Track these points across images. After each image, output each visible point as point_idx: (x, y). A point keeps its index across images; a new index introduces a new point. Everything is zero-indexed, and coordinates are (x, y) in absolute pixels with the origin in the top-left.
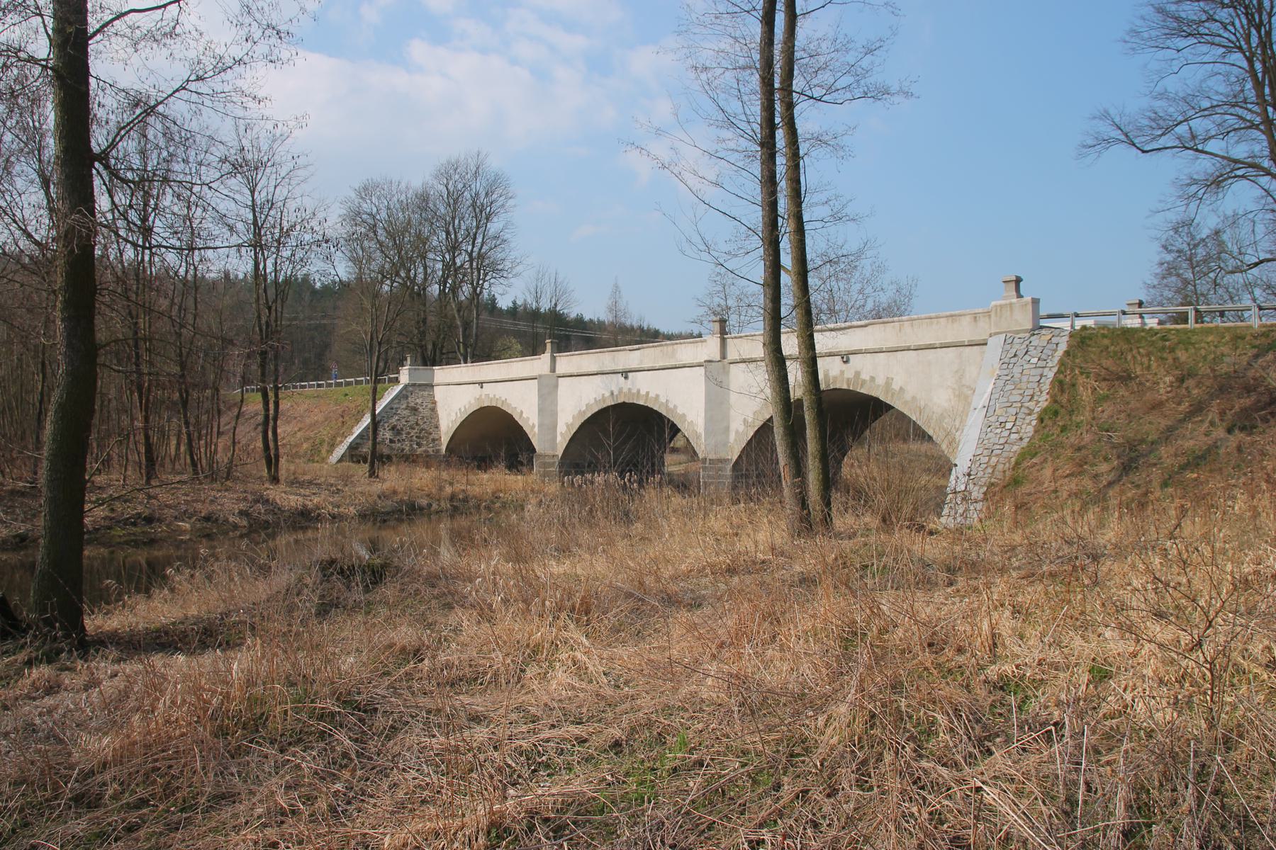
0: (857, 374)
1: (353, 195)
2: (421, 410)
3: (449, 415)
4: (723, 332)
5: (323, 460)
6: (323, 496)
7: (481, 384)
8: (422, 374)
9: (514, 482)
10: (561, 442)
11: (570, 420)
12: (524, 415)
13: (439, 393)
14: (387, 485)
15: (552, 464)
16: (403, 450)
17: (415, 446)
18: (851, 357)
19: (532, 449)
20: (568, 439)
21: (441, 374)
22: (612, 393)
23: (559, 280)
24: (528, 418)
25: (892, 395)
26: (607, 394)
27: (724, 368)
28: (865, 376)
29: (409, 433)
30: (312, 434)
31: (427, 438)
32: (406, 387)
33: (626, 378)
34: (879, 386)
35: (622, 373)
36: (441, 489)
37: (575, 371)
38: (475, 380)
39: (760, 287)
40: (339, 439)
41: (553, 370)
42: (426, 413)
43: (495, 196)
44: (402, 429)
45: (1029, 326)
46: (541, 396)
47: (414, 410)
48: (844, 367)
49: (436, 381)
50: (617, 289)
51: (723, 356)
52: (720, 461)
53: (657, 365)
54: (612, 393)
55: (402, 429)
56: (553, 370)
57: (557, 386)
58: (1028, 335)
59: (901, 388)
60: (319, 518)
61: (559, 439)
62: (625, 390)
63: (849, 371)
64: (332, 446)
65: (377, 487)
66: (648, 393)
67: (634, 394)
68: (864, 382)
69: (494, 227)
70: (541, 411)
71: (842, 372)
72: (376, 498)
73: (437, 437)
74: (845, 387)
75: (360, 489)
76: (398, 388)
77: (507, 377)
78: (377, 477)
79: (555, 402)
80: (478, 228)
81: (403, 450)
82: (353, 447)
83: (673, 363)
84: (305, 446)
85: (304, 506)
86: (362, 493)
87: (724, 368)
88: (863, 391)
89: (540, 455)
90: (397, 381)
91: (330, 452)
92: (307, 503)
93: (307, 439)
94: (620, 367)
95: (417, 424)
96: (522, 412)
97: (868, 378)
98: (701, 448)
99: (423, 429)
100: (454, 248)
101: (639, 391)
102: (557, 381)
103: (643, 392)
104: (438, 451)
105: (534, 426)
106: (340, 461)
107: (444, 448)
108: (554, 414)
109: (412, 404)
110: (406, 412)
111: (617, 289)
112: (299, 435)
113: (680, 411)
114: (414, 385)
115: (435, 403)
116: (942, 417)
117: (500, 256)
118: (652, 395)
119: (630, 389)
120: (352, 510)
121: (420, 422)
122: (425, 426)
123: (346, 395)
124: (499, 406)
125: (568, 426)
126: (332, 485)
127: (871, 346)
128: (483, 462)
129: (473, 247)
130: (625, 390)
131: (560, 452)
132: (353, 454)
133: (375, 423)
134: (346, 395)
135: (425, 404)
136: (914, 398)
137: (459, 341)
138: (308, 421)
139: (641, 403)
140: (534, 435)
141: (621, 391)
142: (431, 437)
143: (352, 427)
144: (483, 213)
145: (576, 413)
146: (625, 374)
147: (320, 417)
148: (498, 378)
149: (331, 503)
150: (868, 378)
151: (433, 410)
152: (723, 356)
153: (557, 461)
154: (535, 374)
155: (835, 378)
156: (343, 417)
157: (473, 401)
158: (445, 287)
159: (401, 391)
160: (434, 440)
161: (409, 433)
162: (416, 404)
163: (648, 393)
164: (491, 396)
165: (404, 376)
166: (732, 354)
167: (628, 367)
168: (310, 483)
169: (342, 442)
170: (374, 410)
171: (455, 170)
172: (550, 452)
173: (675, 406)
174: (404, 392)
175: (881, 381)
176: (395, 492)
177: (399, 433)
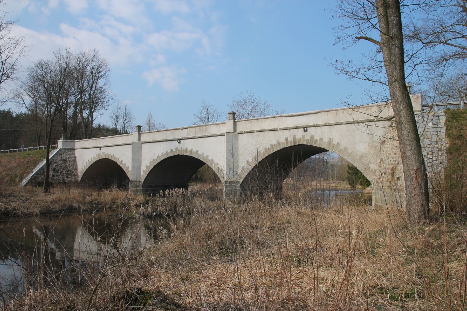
0: (312, 137)
1: (34, 66)
2: (68, 160)
3: (83, 163)
4: (234, 119)
5: (17, 185)
6: (18, 202)
7: (100, 148)
8: (69, 144)
9: (121, 195)
10: (143, 175)
11: (148, 164)
12: (123, 162)
13: (77, 153)
14: (56, 196)
15: (139, 186)
16: (59, 180)
17: (65, 178)
18: (308, 128)
19: (127, 178)
20: (147, 174)
21: (78, 144)
22: (172, 150)
23: (127, 109)
24: (125, 164)
25: (333, 147)
26: (169, 151)
27: (236, 136)
28: (316, 138)
29: (62, 172)
30: (11, 173)
31: (71, 174)
32: (61, 149)
33: (179, 143)
34: (325, 143)
35: (178, 140)
36: (84, 198)
37: (151, 140)
38: (97, 146)
39: (375, 47)
40: (25, 175)
41: (139, 140)
42: (71, 162)
43: (101, 70)
44: (59, 170)
45: (420, 109)
46: (133, 152)
47: (65, 161)
48: (305, 133)
49: (76, 147)
50: (150, 115)
51: (235, 130)
52: (234, 182)
53: (197, 136)
54: (172, 150)
55: (59, 170)
56: (139, 140)
57: (141, 148)
58: (420, 113)
59: (338, 143)
60: (16, 216)
61: (142, 173)
62: (179, 149)
63: (307, 136)
64: (22, 179)
65: (50, 198)
66: (192, 150)
67: (184, 151)
68: (316, 141)
69: (101, 83)
70: (133, 160)
71: (304, 136)
72: (49, 203)
73: (76, 174)
74: (305, 143)
75: (40, 199)
76: (56, 151)
77: (114, 144)
78: (49, 192)
79: (140, 155)
80: (93, 83)
81: (59, 180)
82: (33, 178)
83: (206, 134)
84: (7, 178)
85: (6, 208)
86: (41, 201)
87: (236, 136)
88: (315, 145)
89: (132, 182)
90: (55, 148)
91: (20, 181)
92: (7, 206)
93: (8, 175)
94: (176, 137)
95: (66, 167)
96: (122, 161)
97: (318, 139)
98: (224, 176)
99: (69, 170)
100: (82, 92)
101: (187, 149)
102: (142, 145)
103: (189, 149)
104: (77, 181)
105: (128, 167)
106: (26, 185)
107: (79, 179)
108: (140, 162)
109: (64, 158)
110: (61, 162)
111: (150, 115)
112: (3, 173)
113: (210, 158)
114: (65, 149)
115: (75, 157)
116: (362, 157)
117: (104, 96)
118: (194, 150)
119: (181, 148)
120: (37, 211)
121: (68, 167)
122: (70, 169)
123: (29, 154)
124: (110, 158)
125: (147, 167)
126: (23, 197)
127: (320, 123)
128: (107, 185)
129: (91, 91)
130: (179, 149)
131: (142, 180)
132: (34, 182)
133: (49, 163)
134: (29, 154)
135: (70, 158)
136: (345, 148)
137: (83, 133)
138: (9, 167)
139: (188, 154)
140: (129, 171)
141: (176, 149)
142: (73, 174)
143: (33, 169)
144: (96, 79)
145: (152, 160)
146: (179, 141)
147: (15, 165)
148: (109, 144)
149: (24, 207)
150: (318, 139)
151: (75, 161)
152: (235, 130)
153: (141, 184)
154: (130, 142)
155: (299, 139)
156: (27, 164)
157: (96, 156)
158: (76, 108)
159: (58, 152)
160: (75, 175)
161: (62, 172)
162: (66, 158)
163: (192, 150)
164: (106, 153)
165: (60, 144)
166: (239, 129)
167: (180, 137)
168: (10, 195)
169: (27, 176)
170: (48, 156)
171: (84, 57)
172: (138, 180)
173: (207, 156)
174: (60, 152)
175: (326, 140)
176: (60, 200)
177: (57, 172)
